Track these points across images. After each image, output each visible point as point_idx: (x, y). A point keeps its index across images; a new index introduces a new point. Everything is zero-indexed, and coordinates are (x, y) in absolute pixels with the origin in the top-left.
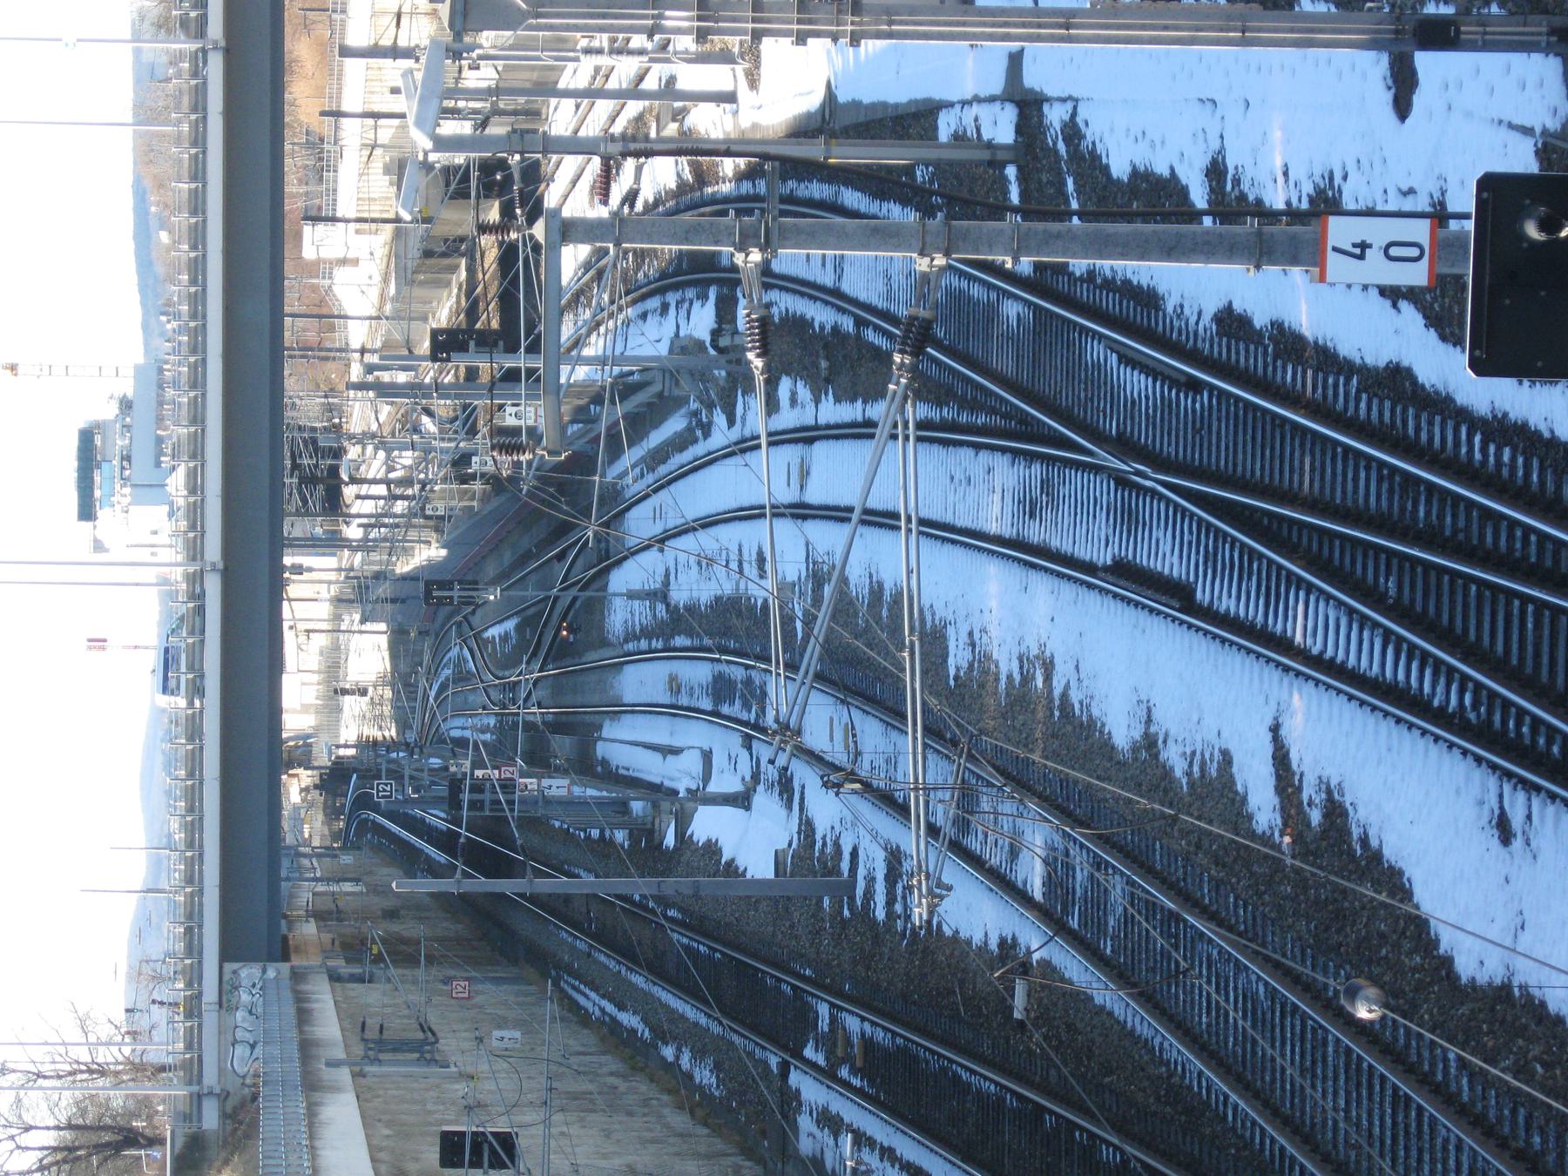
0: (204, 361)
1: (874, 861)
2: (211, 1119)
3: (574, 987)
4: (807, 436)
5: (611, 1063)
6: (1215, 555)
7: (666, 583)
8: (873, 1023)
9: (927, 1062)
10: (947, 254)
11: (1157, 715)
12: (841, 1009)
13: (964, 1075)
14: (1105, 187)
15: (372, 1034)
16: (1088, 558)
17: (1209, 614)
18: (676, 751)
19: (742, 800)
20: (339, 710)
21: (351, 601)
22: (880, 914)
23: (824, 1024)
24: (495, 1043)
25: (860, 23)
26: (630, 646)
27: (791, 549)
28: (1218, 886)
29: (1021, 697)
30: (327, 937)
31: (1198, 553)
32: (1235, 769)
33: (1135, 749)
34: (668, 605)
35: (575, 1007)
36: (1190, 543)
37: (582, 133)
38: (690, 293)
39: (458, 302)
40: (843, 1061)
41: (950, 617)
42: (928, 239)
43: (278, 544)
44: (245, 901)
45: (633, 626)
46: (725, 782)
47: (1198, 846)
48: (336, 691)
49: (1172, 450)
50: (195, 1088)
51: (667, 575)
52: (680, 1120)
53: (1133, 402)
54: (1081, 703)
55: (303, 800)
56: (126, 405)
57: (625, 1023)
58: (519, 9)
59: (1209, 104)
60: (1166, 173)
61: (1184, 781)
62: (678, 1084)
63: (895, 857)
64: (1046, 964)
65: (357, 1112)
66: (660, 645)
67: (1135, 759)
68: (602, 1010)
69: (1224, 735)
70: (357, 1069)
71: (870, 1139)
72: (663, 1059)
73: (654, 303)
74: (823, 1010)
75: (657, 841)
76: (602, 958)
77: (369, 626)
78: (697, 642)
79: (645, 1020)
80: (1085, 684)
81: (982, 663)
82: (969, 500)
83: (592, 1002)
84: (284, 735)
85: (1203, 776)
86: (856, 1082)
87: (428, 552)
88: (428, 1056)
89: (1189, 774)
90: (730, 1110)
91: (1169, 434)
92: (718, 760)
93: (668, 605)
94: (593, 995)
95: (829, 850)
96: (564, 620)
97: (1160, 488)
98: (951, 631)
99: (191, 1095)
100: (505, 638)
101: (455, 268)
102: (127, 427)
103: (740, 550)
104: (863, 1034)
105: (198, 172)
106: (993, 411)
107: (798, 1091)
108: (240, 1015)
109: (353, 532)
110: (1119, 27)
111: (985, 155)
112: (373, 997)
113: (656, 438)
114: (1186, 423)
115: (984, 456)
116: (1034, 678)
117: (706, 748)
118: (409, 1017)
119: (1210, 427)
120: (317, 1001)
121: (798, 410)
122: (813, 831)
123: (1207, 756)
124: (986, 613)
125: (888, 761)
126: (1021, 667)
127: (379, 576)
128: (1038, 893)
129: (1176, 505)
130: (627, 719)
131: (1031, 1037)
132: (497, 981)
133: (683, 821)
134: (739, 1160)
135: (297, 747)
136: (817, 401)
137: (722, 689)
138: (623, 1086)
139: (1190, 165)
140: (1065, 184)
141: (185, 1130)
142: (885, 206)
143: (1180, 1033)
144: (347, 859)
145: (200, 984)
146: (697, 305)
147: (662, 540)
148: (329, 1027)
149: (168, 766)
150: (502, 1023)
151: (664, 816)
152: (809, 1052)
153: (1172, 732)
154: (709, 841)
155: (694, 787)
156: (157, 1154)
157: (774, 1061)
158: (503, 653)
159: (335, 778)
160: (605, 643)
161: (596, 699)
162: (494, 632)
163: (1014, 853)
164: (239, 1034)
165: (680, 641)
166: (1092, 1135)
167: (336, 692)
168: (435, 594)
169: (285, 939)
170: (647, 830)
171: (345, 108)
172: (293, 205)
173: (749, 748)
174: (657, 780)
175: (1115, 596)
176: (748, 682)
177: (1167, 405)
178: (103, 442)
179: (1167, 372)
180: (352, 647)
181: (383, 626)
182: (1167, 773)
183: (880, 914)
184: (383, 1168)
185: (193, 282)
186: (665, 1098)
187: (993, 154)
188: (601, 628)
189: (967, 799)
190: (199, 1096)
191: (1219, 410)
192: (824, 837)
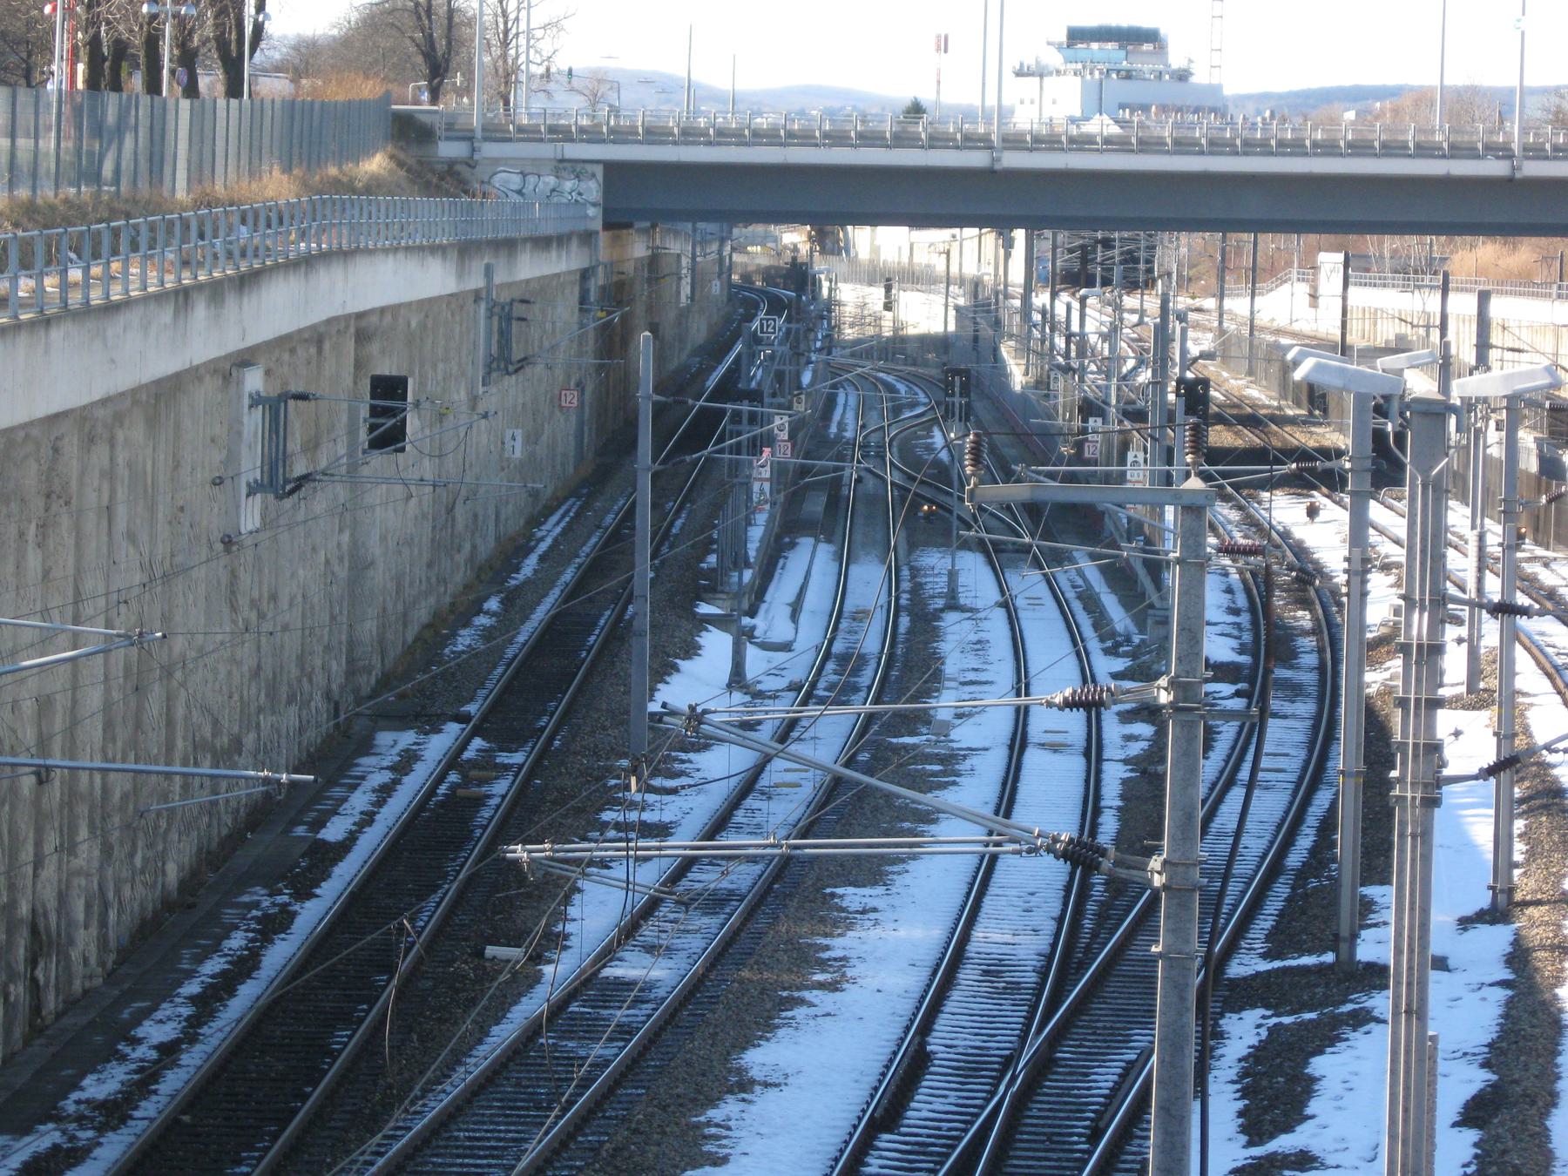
0: (1202, 153)
1: (663, 810)
2: (448, 150)
3: (568, 511)
4: (1093, 752)
5: (486, 547)
6: (924, 1154)
7: (962, 609)
8: (498, 807)
9: (453, 860)
10: (1165, 887)
11: (772, 1093)
12: (516, 776)
13: (436, 897)
14: (1302, 1050)
15: (519, 309)
16: (936, 1027)
17: (864, 1146)
18: (795, 615)
19: (737, 679)
20: (871, 283)
21: (976, 296)
22: (607, 816)
23: (504, 758)
24: (509, 433)
25: (1413, 806)
26: (905, 572)
27: (983, 733)
28: (592, 1150)
29: (806, 958)
30: (629, 268)
31: (929, 1136)
32: (707, 1168)
33: (740, 1071)
34: (942, 610)
35: (549, 511)
36: (939, 1129)
37: (1371, 531)
38: (1247, 637)
39: (1264, 407)
40: (464, 776)
41: (894, 890)
42: (1181, 869)
43: (1034, 225)
44: (670, 187)
45: (926, 576)
46: (756, 662)
47: (636, 1131)
48: (889, 280)
49: (1035, 1113)
50: (479, 134)
51: (971, 610)
52: (422, 614)
53: (1087, 1075)
54: (793, 1018)
55: (785, 247)
56: (1183, 76)
57: (527, 562)
58: (1432, 468)
59: (1370, 1155)
60: (1308, 1111)
61: (702, 1119)
62: (463, 613)
63: (662, 830)
64: (537, 978)
65: (436, 294)
66: (903, 602)
67: (730, 1071)
68: (542, 539)
69: (745, 1160)
70: (484, 295)
71: (385, 801)
72: (486, 599)
73: (1241, 601)
74: (518, 758)
75: (704, 596)
76: (594, 540)
77: (952, 313)
78: (901, 638)
79: (527, 582)
80: (812, 1023)
81: (843, 921)
82: (1009, 911)
83: (551, 530)
84: (850, 228)
85: (705, 1137)
86: (442, 789)
87: (1018, 375)
88: (494, 365)
89: (709, 1124)
90: (429, 663)
91: (1050, 1110)
92: (780, 657)
93: (942, 610)
94: (558, 530)
95: (677, 766)
96: (939, 506)
97: (996, 1099)
98: (880, 890)
99: (472, 131)
100: (930, 448)
101: (1298, 404)
102: (1160, 75)
103: (986, 683)
104: (490, 797)
105: (1392, 149)
106: (1095, 935)
107: (439, 731)
108: (551, 180)
109: (1041, 299)
110: (1407, 1062)
111: (1345, 932)
112: (565, 311)
113: (1110, 602)
114: (1060, 1126)
115: (1050, 926)
116: (823, 971)
117: (795, 646)
118: (541, 347)
119: (1053, 1150)
120: (559, 257)
121: (1120, 742)
122: (698, 751)
123: (724, 1142)
124: (894, 925)
125: (759, 826)
126: (835, 959)
127: (997, 323)
128: (607, 972)
129: (977, 1115)
130: (834, 567)
131: (466, 962)
132: (579, 436)
133: (721, 622)
134: (377, 672)
135: (838, 240)
136: (1126, 761)
137: (851, 662)
138: (461, 558)
139: (1314, 1135)
140: (1311, 1011)
141: (439, 126)
142: (1312, 832)
143: (451, 1109)
144: (716, 287)
145: (582, 141)
146: (1234, 643)
147: (1008, 606)
148: (529, 267)
149: (830, 113)
150: (532, 439)
151: (728, 604)
152: (478, 743)
153: (753, 1108)
154: (700, 647)
155: (756, 633)
156: (425, 97)
157: (472, 708)
158: (917, 446)
159: (799, 276)
160: (912, 546)
161: (858, 537)
162: (938, 439)
163: (650, 949)
164: (532, 179)
165: (905, 621)
166: (362, 1020)
167: (888, 280)
168: (957, 378)
169: (629, 226)
170: (703, 582)
171: (1452, 296)
172: (1371, 244)
173: (790, 688)
174: (768, 597)
175: (895, 1053)
176: (855, 689)
177: (1081, 1108)
178: (1147, 52)
179: (1111, 1109)
180: (932, 296)
181: (952, 327)
182: (712, 1102)
183: (607, 816)
184: (374, 319)
185: (1315, 144)
186: (448, 599)
187: (1345, 940)
188: (927, 544)
189: (715, 902)
190: (471, 139)
191: (1068, 1160)
192: (690, 762)
